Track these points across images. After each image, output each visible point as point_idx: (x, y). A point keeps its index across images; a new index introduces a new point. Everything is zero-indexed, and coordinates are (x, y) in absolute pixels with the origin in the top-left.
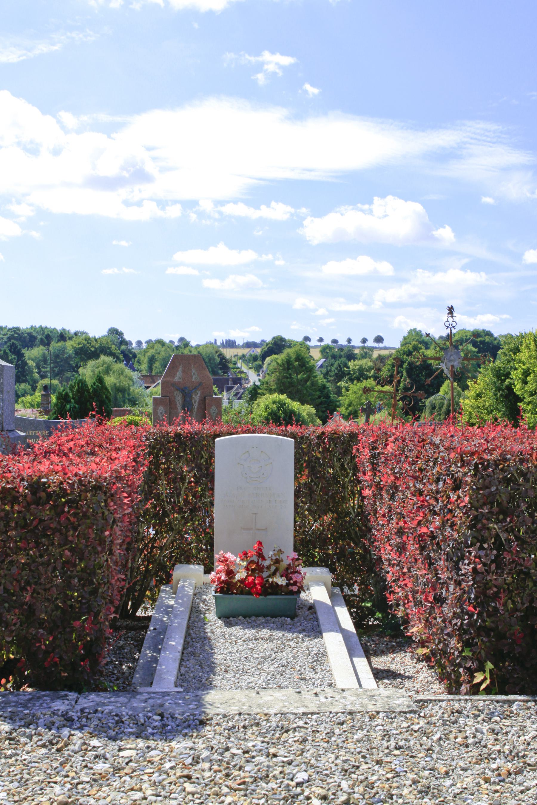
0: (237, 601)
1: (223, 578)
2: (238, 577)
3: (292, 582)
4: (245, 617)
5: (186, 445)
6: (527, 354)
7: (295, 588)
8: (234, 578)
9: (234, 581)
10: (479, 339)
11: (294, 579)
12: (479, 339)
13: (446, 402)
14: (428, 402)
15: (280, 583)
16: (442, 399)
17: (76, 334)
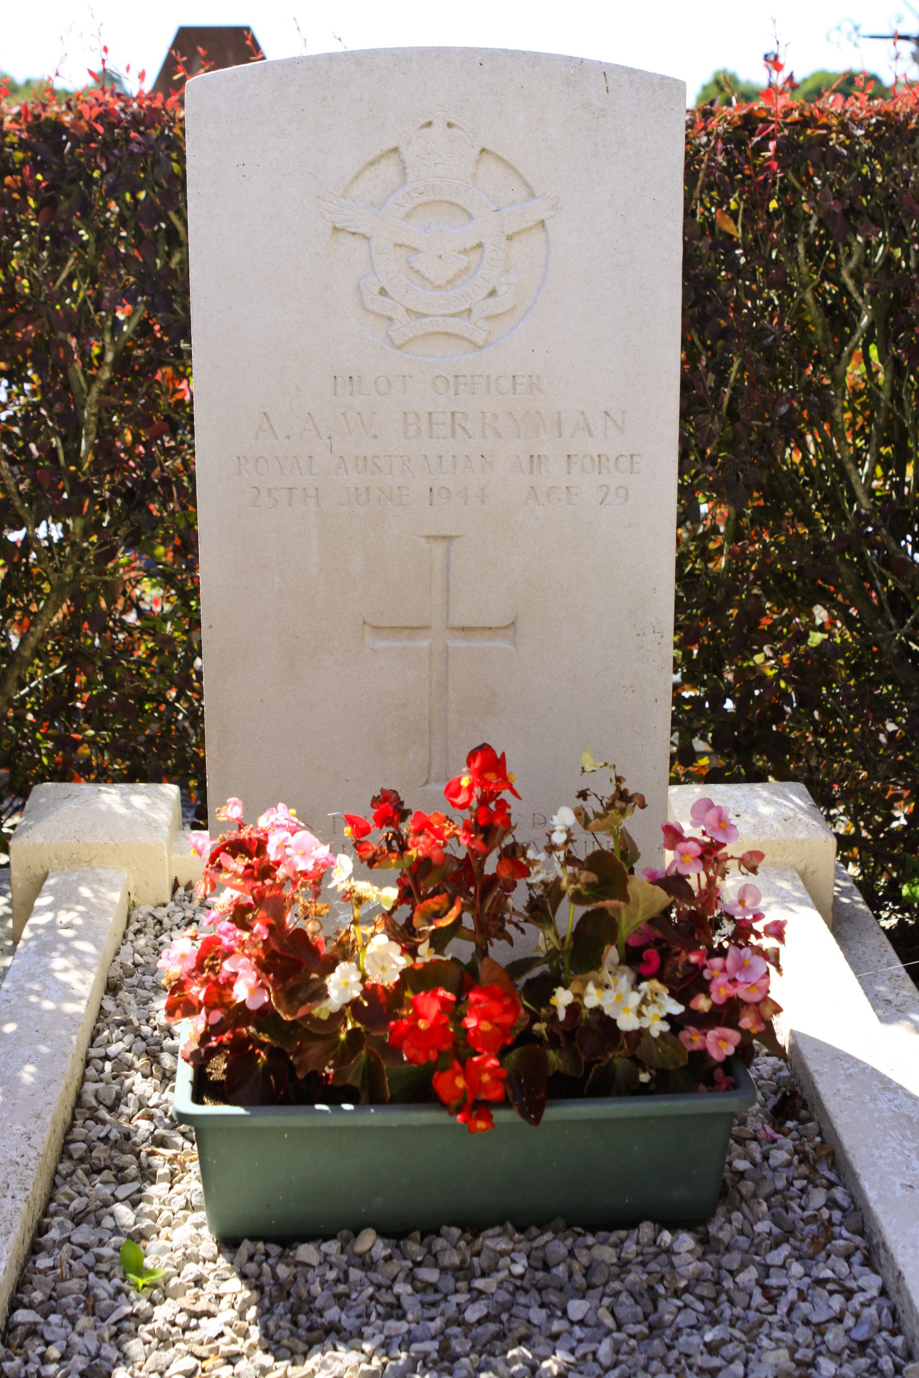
0: (336, 1142)
1: (241, 992)
2: (341, 986)
3: (703, 1004)
4: (395, 1233)
5: (90, 181)
7: (720, 1044)
8: (321, 994)
9: (322, 1011)
11: (720, 991)
15: (627, 1022)
17: (28, 83)
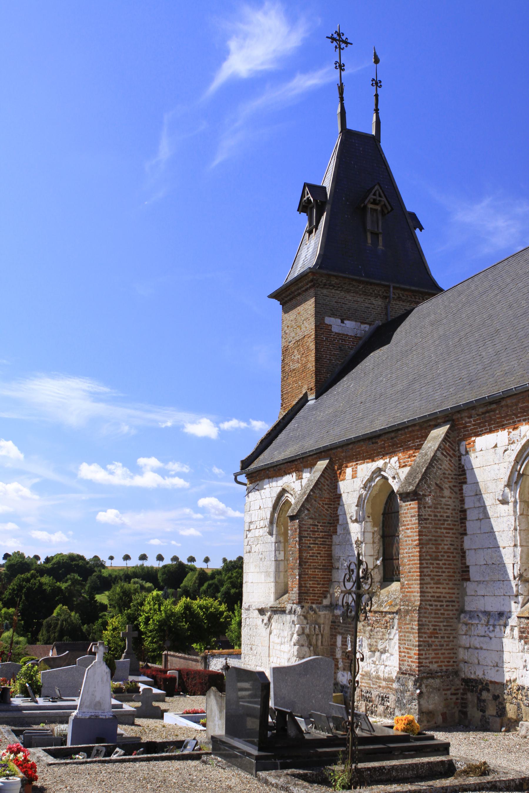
6: (148, 608)
10: (74, 563)
12: (74, 563)
13: (59, 622)
14: (44, 622)
16: (56, 620)
